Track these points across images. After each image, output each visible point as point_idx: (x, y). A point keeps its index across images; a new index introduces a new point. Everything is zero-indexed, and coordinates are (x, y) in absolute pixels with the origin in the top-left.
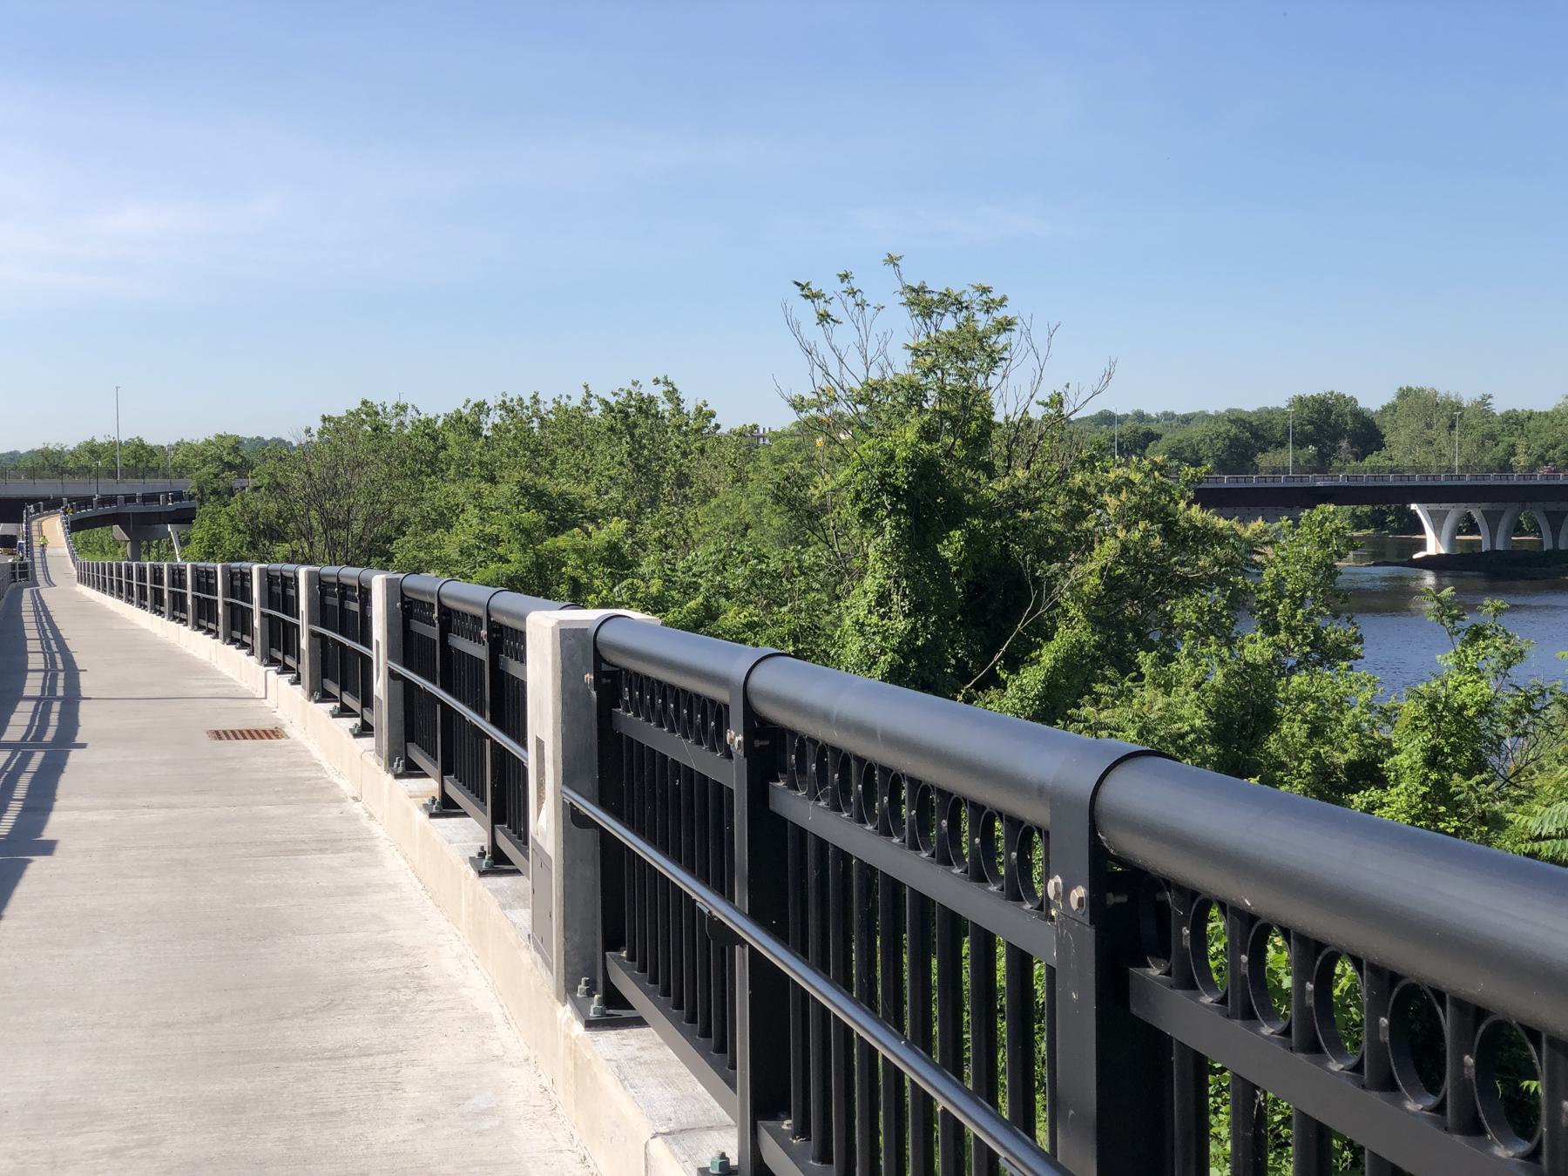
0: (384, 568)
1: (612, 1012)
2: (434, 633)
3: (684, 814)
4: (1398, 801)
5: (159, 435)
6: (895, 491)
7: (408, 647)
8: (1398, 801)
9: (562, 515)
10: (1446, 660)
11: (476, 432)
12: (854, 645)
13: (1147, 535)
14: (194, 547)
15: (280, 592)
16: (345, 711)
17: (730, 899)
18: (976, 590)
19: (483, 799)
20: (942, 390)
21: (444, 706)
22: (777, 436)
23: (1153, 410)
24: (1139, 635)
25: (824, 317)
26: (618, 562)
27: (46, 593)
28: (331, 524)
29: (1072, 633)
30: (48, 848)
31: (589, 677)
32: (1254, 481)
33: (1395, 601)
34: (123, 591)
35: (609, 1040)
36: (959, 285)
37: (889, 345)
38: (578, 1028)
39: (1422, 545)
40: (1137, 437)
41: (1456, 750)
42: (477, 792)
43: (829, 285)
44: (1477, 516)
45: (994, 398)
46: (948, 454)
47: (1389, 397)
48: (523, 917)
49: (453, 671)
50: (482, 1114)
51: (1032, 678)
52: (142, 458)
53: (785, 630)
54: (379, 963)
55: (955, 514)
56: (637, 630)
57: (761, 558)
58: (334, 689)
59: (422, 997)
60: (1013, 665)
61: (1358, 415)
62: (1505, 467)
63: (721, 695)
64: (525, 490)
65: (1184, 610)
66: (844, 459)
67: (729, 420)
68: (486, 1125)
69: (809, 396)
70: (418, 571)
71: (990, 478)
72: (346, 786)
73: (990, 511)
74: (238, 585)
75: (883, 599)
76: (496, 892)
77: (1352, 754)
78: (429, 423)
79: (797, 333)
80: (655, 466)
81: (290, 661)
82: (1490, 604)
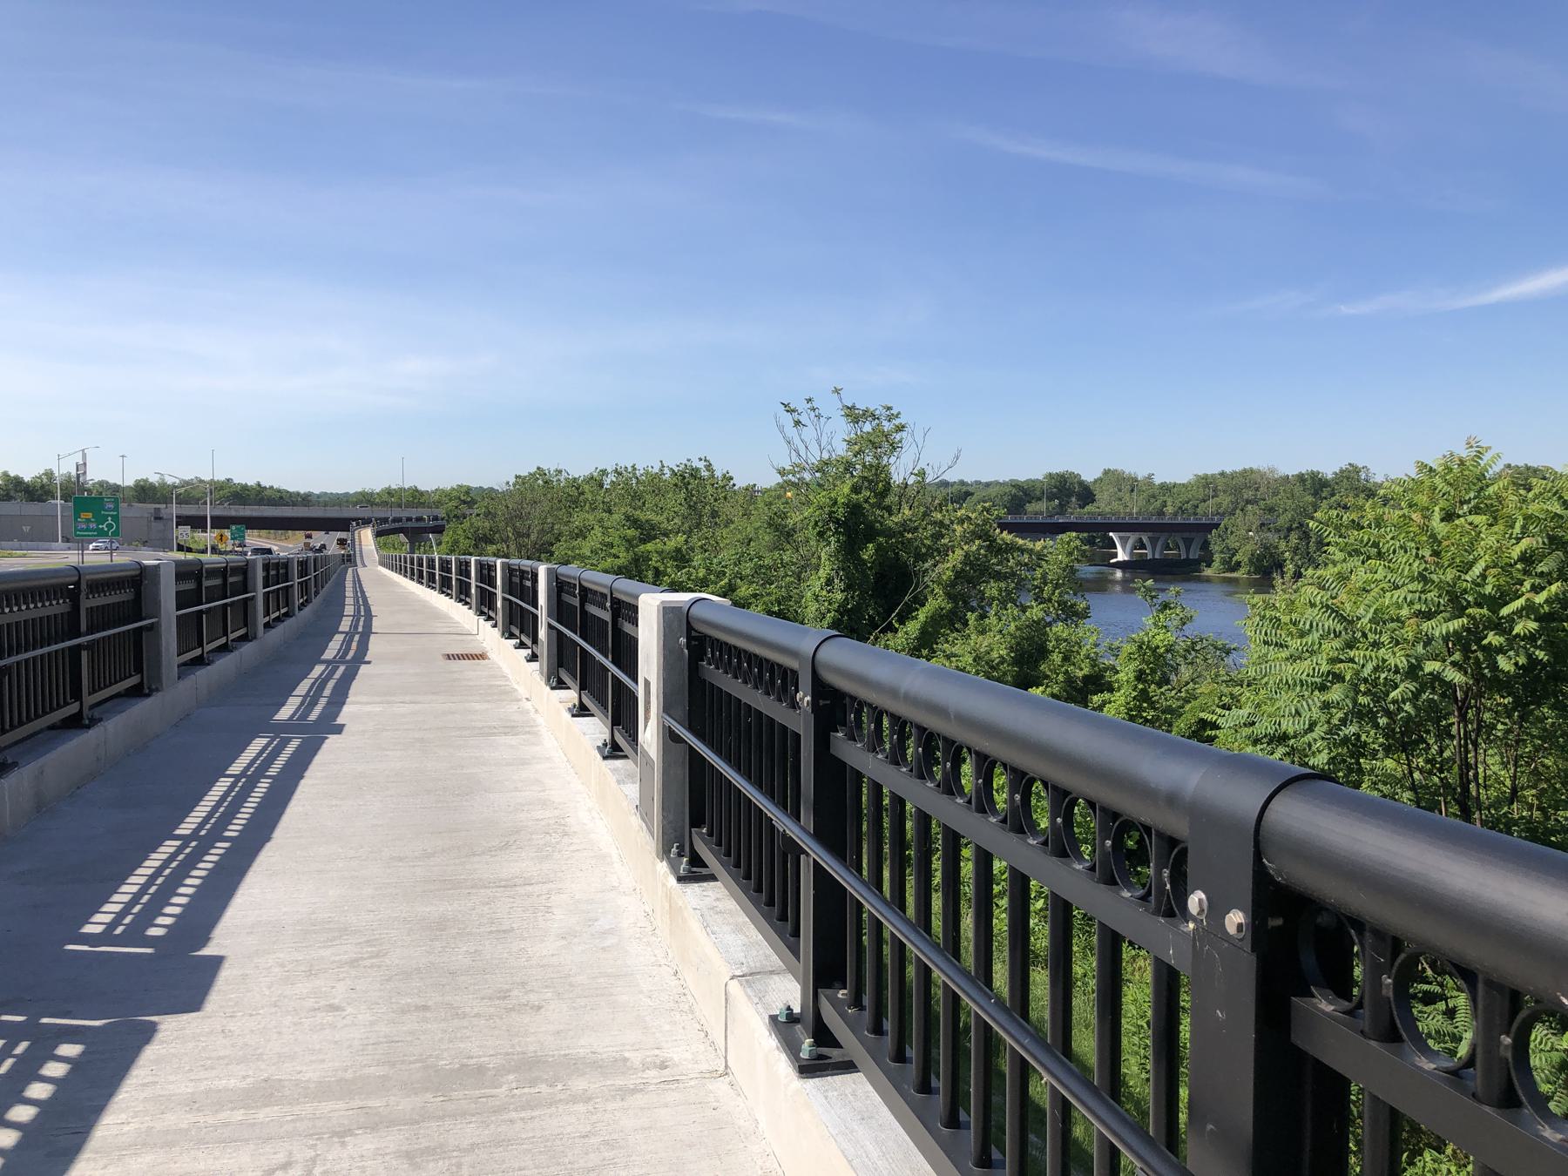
0: (548, 561)
1: (694, 872)
2: (576, 602)
3: (764, 749)
4: (1117, 703)
5: (427, 484)
6: (837, 521)
7: (560, 610)
8: (1117, 703)
9: (648, 532)
10: (1148, 621)
11: (601, 486)
12: (812, 608)
13: (980, 547)
14: (443, 546)
15: (486, 574)
16: (522, 645)
17: (796, 816)
18: (880, 577)
19: (606, 708)
20: (864, 466)
21: (582, 649)
22: (766, 491)
23: (969, 480)
24: (965, 603)
25: (798, 423)
26: (681, 558)
27: (361, 571)
28: (519, 535)
29: (936, 602)
30: (339, 729)
31: (683, 640)
32: (1025, 519)
33: (1101, 585)
34: (401, 570)
35: (694, 889)
36: (875, 405)
37: (836, 439)
38: (672, 880)
39: (1115, 555)
40: (962, 494)
41: (1153, 671)
42: (603, 704)
43: (801, 406)
44: (1145, 540)
45: (892, 469)
46: (866, 501)
47: (1099, 474)
48: (633, 790)
49: (588, 627)
50: (604, 933)
51: (913, 628)
52: (416, 497)
53: (773, 598)
54: (539, 814)
55: (871, 534)
56: (712, 606)
57: (760, 558)
58: (517, 632)
59: (566, 840)
60: (902, 620)
61: (1081, 483)
62: (1161, 513)
63: (792, 664)
64: (628, 518)
65: (992, 589)
66: (809, 503)
67: (740, 482)
68: (607, 943)
69: (788, 468)
70: (567, 563)
71: (890, 515)
72: (522, 691)
73: (889, 533)
74: (464, 569)
75: (829, 582)
76: (614, 771)
77: (1086, 671)
78: (575, 480)
79: (782, 432)
80: (699, 506)
81: (492, 614)
82: (1173, 589)
